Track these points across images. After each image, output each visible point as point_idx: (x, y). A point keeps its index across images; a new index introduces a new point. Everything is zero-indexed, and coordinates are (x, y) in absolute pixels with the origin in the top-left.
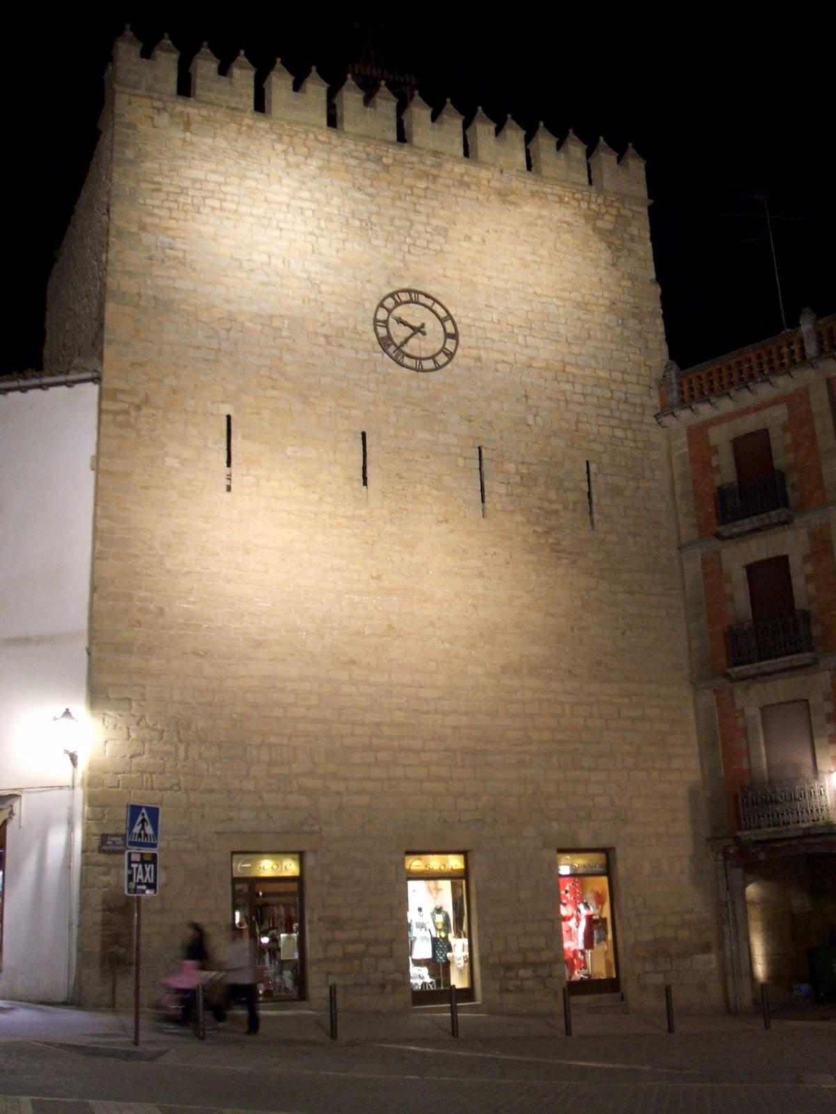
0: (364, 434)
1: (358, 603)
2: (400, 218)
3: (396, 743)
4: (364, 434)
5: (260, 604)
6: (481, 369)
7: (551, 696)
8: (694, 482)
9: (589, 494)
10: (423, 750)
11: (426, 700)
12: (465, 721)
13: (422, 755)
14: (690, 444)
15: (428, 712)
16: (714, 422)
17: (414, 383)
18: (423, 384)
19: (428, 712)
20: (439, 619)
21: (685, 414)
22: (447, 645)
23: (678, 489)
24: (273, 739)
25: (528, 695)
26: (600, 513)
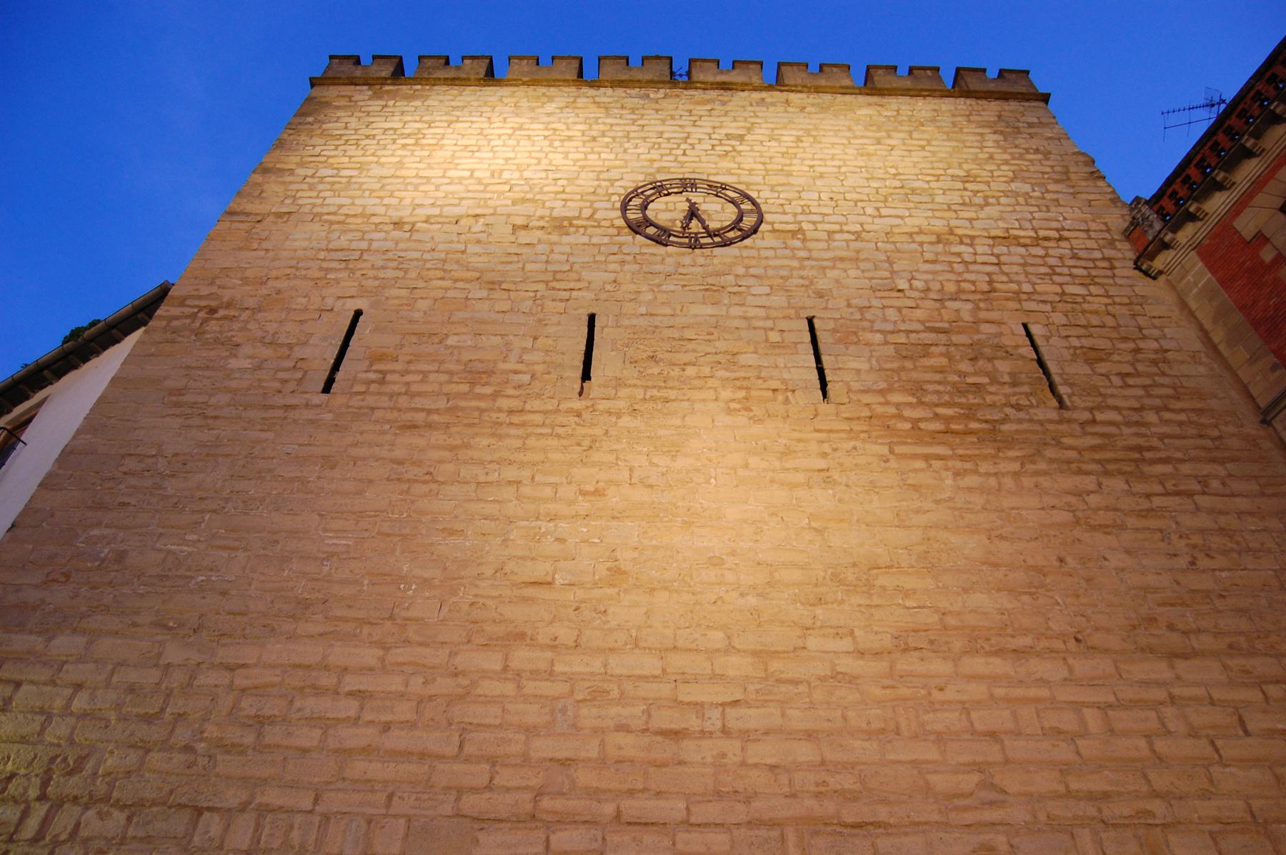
0: (592, 318)
1: (545, 535)
2: (485, 674)
3: (609, 809)
4: (592, 318)
5: (330, 542)
6: (759, 625)
7: (1044, 693)
8: (1242, 308)
9: (1041, 363)
10: (688, 824)
11: (699, 707)
12: (805, 752)
13: (682, 836)
14: (1211, 266)
15: (704, 734)
16: (1238, 208)
17: (687, 260)
18: (701, 261)
19: (704, 734)
20: (733, 553)
21: (1187, 234)
22: (752, 600)
23: (1218, 336)
24: (273, 797)
25: (977, 691)
26: (1066, 383)
